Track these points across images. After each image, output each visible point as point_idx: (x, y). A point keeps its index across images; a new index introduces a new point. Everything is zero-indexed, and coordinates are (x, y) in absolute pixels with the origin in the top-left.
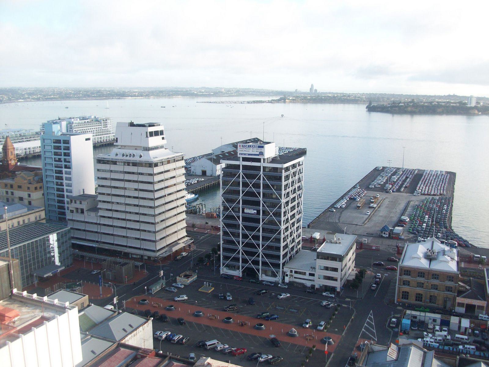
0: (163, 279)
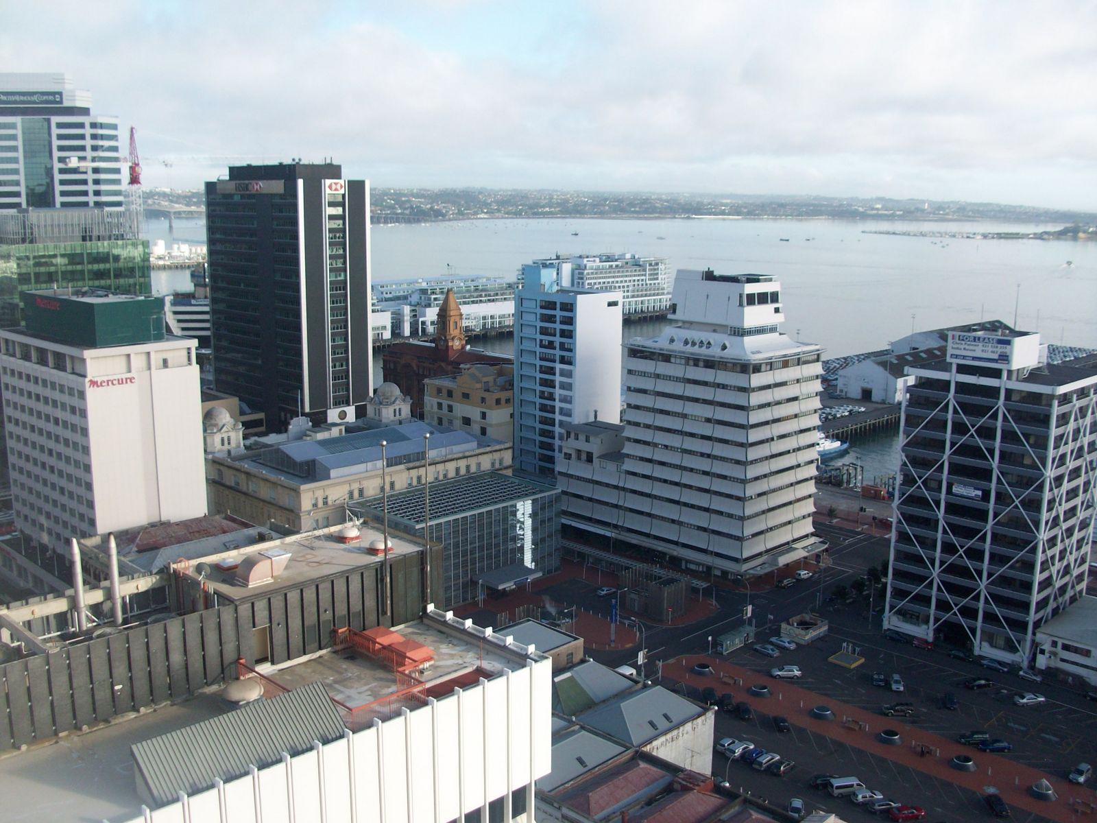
0: (750, 624)
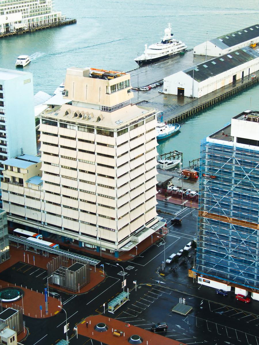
0: (126, 291)
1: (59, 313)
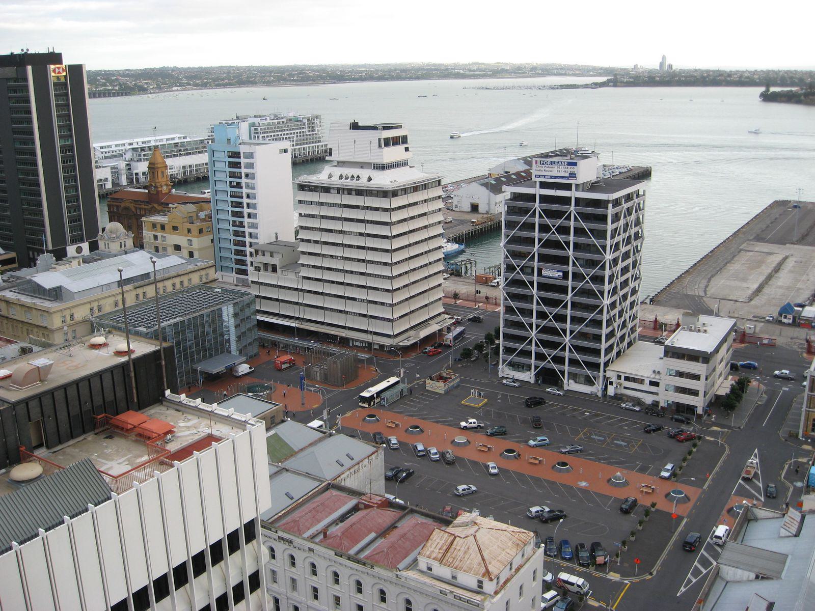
1: (318, 407)
